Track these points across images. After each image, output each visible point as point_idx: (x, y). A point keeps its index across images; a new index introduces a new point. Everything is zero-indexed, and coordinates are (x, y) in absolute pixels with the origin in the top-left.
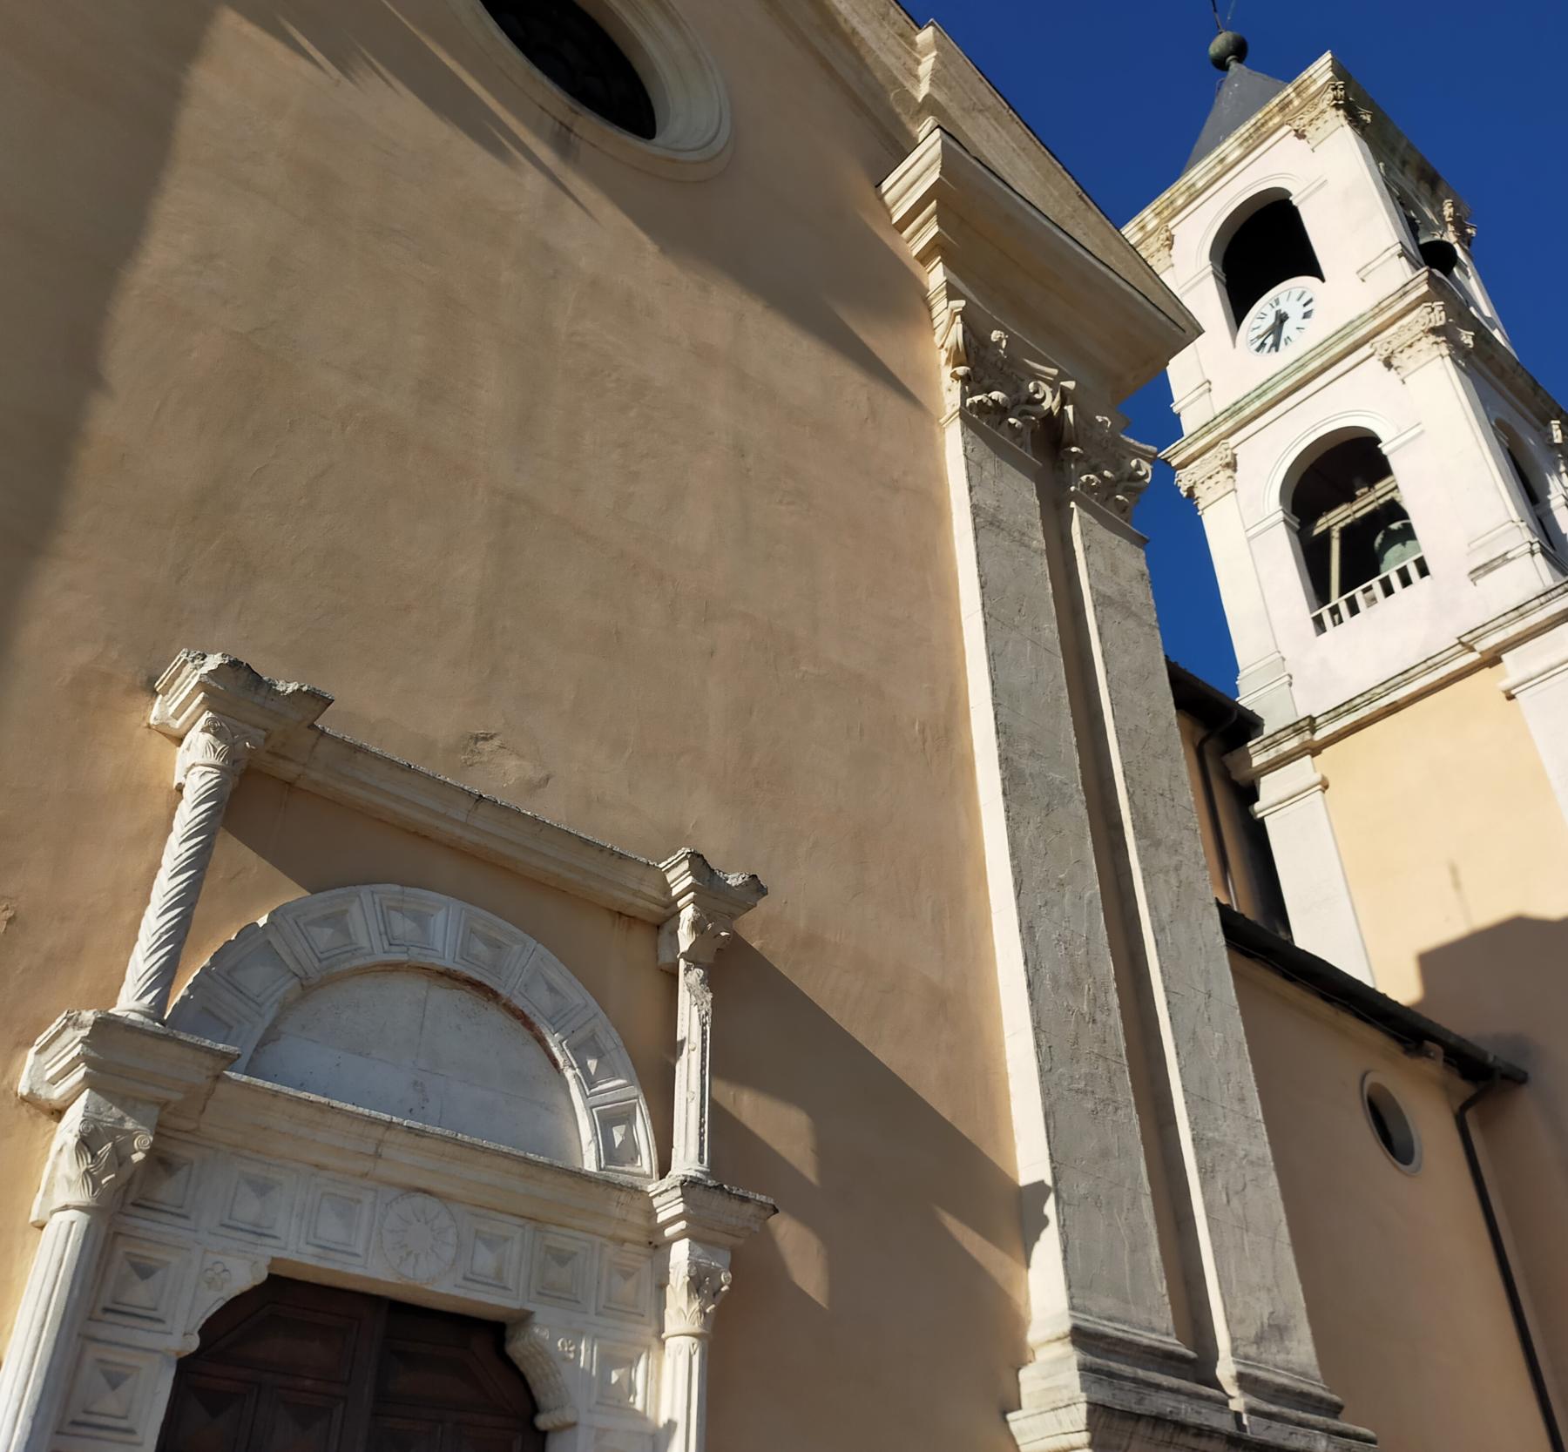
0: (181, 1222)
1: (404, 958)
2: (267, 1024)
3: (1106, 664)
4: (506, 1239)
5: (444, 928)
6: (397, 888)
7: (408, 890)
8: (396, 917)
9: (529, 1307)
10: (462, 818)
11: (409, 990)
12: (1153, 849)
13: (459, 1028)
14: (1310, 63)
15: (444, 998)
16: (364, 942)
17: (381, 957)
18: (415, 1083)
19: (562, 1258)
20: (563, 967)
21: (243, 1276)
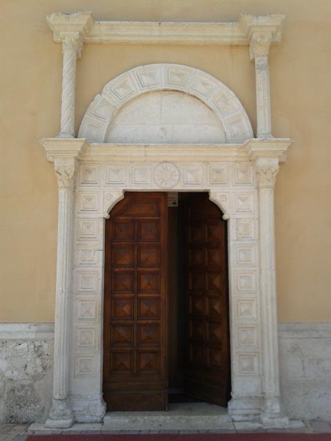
0: (95, 185)
1: (148, 90)
2: (108, 123)
3: (273, 110)
4: (198, 170)
5: (160, 74)
6: (141, 67)
7: (146, 66)
8: (143, 77)
9: (208, 188)
10: (157, 34)
11: (153, 100)
12: (278, 38)
13: (174, 107)
14: (138, 436)
15: (168, 98)
16: (133, 89)
17: (140, 92)
18: (162, 129)
19: (218, 172)
20: (207, 75)
21: (117, 196)
